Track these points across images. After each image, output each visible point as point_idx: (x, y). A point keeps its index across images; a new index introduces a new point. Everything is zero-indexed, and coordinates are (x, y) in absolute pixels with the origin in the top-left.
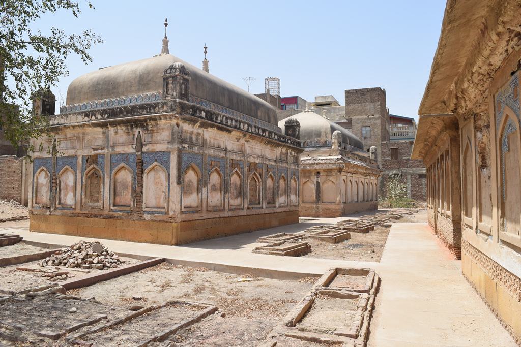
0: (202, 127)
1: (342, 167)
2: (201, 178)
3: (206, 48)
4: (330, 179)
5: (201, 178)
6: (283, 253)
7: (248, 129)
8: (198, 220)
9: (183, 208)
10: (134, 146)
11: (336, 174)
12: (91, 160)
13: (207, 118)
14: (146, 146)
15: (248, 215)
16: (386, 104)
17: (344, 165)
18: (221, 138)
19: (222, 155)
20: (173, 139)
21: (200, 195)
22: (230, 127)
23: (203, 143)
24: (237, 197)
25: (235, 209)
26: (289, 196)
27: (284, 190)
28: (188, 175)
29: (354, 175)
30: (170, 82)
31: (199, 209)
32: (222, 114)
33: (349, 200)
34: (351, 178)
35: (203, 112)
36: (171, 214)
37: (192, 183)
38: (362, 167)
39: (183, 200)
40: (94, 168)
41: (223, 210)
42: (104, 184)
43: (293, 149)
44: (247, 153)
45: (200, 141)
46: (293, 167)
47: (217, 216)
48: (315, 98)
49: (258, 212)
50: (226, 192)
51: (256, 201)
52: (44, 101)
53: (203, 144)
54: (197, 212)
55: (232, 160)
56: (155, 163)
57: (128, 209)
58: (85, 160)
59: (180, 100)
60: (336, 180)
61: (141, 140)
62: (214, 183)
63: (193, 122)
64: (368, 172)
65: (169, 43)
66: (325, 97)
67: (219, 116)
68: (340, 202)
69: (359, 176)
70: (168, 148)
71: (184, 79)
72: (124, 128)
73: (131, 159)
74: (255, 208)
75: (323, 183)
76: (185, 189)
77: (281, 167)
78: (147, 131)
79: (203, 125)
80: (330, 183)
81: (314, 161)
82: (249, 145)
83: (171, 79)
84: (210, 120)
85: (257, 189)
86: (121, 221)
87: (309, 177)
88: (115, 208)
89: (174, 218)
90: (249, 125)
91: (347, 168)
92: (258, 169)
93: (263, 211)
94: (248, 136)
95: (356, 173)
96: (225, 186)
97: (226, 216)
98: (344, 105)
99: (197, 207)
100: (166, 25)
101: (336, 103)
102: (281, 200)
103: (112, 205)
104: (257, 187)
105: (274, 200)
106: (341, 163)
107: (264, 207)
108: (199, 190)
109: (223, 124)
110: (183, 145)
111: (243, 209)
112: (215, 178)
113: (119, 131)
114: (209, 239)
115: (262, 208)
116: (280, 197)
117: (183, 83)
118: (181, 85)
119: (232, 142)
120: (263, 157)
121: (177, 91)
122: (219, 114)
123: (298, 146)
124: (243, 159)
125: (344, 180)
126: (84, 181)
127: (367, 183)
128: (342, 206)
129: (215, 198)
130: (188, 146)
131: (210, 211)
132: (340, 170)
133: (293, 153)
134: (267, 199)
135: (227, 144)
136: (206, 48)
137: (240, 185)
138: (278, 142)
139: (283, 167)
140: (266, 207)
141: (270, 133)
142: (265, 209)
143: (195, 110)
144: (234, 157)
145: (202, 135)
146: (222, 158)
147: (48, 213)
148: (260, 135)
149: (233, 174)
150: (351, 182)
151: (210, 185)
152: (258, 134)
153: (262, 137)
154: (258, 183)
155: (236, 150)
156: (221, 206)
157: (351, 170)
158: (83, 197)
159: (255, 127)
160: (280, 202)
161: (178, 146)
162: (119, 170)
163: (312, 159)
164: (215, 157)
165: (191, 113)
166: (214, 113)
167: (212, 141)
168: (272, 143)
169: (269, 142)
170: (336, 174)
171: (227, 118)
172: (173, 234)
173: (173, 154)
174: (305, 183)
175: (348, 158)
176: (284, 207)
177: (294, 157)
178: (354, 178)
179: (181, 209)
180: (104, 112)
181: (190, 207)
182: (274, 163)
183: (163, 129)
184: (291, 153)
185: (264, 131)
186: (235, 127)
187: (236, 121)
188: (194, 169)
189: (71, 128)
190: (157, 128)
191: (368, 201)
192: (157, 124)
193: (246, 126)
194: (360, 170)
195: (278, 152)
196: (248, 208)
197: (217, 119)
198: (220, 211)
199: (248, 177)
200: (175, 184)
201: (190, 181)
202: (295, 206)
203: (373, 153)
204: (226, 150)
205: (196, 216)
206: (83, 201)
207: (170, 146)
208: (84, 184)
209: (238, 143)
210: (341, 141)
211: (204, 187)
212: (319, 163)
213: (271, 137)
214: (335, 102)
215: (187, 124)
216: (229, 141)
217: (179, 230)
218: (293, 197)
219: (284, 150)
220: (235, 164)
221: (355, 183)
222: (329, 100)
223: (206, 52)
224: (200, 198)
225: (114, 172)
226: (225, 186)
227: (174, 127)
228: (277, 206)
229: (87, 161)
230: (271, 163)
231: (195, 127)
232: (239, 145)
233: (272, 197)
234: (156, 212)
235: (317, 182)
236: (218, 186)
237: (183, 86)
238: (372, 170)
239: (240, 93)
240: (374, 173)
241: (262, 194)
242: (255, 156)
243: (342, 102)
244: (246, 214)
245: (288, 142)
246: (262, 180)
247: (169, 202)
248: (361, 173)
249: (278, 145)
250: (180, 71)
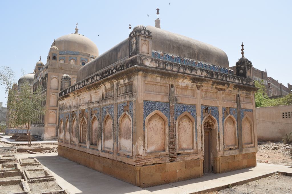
3: (158, 10)
15: (78, 150)
77: (105, 105)
97: (76, 149)
107: (88, 147)
133: (122, 81)
136: (158, 10)
139: (108, 105)
140: (90, 148)
176: (109, 152)
177: (125, 85)
182: (97, 105)
195: (101, 91)
219: (108, 85)
223: (158, 13)
230: (94, 105)
244: (77, 150)
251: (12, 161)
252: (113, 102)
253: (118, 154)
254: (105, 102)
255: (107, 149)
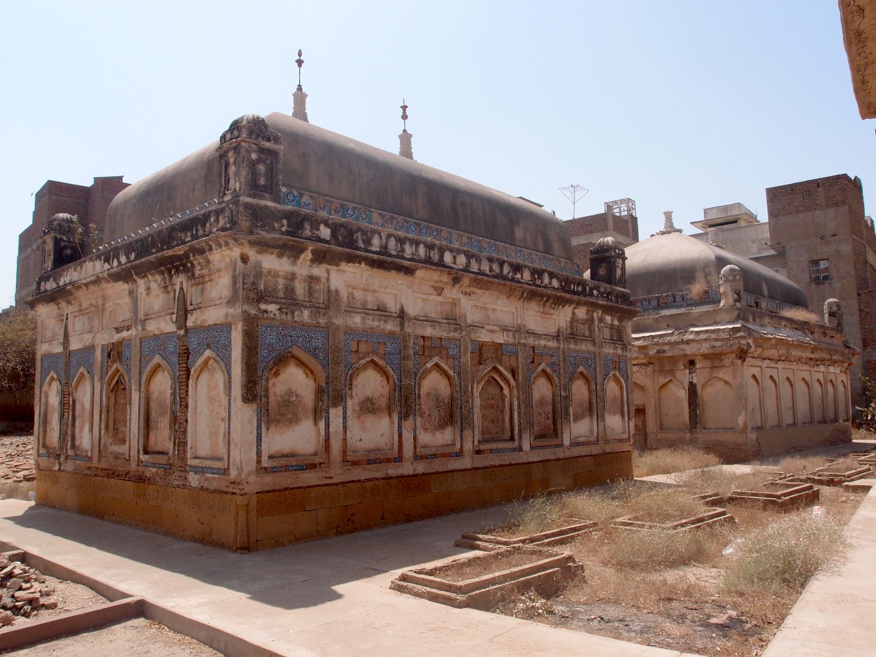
0: (321, 262)
1: (745, 348)
2: (323, 385)
3: (404, 108)
4: (720, 376)
5: (323, 385)
6: (460, 597)
7: (468, 264)
8: (318, 486)
9: (265, 458)
10: (174, 316)
11: (733, 364)
12: (114, 352)
13: (337, 240)
14: (192, 314)
15: (477, 468)
16: (864, 210)
17: (750, 341)
18: (386, 287)
19: (390, 326)
20: (235, 291)
21: (322, 424)
22: (410, 260)
23: (329, 300)
24: (442, 426)
25: (435, 456)
26: (601, 418)
27: (587, 405)
28: (283, 377)
29: (780, 365)
30: (232, 160)
31: (317, 460)
32: (383, 233)
33: (772, 420)
34: (769, 372)
35: (322, 227)
36: (233, 474)
37: (297, 396)
38: (801, 346)
39: (264, 439)
40: (117, 371)
41: (399, 459)
42: (130, 404)
43: (607, 310)
44: (469, 321)
45: (321, 298)
46: (609, 350)
47: (378, 475)
48: (705, 213)
49: (506, 459)
50: (405, 415)
51: (497, 433)
52: (57, 242)
53: (332, 300)
54: (312, 466)
55: (423, 337)
56: (208, 353)
57: (163, 459)
58: (106, 354)
59: (249, 200)
60: (734, 377)
61: (185, 301)
62: (369, 393)
63: (293, 251)
64: (817, 355)
65: (412, 139)
66: (726, 208)
67: (376, 236)
68: (745, 427)
69: (794, 366)
70: (227, 315)
71: (261, 150)
72: (158, 278)
73: (171, 347)
74: (498, 451)
75: (703, 386)
76: (271, 413)
77: (575, 350)
78: (195, 279)
79: (320, 257)
80: (720, 385)
81: (681, 337)
82: (472, 303)
83: (231, 154)
84: (347, 246)
85: (504, 406)
86: (155, 487)
87: (672, 372)
88: (147, 456)
89: (239, 483)
90: (469, 256)
91: (759, 350)
92: (505, 359)
93: (522, 458)
94: (466, 281)
95: (787, 360)
96: (404, 402)
98: (767, 221)
99: (315, 454)
100: (300, 63)
101: (751, 219)
102: (579, 429)
103: (141, 452)
104: (503, 401)
105: (555, 430)
106: (741, 337)
107: (526, 446)
108: (319, 413)
109: (391, 256)
110: (263, 306)
111: (460, 454)
112: (370, 384)
113: (153, 285)
114: (354, 530)
115: (520, 449)
116: (575, 421)
117: (259, 161)
118: (253, 165)
119: (420, 296)
120: (519, 330)
121: (242, 179)
122: (373, 232)
123: (622, 303)
124: (457, 335)
125: (754, 376)
126: (104, 399)
127: (818, 380)
128: (752, 436)
129: (374, 433)
130: (280, 309)
131: (355, 463)
132: (742, 354)
133: (608, 319)
134: (536, 428)
135: (403, 301)
136: (404, 108)
137: (452, 398)
138: (559, 294)
140: (532, 448)
141: (537, 273)
142: (527, 450)
143: (297, 222)
144: (429, 331)
145: (323, 280)
146: (392, 334)
147: (57, 468)
148: (505, 278)
149: (430, 371)
150: (820, 383)
151: (356, 400)
152: (500, 276)
153: (508, 283)
154: (506, 391)
155: (433, 315)
156: (392, 448)
157: (773, 353)
158: (103, 432)
159: (490, 260)
160: (574, 434)
161: (246, 307)
162: (154, 371)
163: (676, 332)
164: (367, 333)
165: (284, 229)
166: (359, 229)
167: (359, 295)
168: (542, 296)
169: (533, 295)
170: (733, 364)
171: (401, 241)
172: (237, 524)
173: (236, 329)
174: (664, 386)
175: (762, 326)
176: (588, 443)
177: (612, 327)
178: (781, 371)
179: (259, 462)
180: (129, 248)
181: (292, 455)
182: (552, 344)
183: (219, 271)
184: (601, 320)
185: (517, 268)
186: (428, 261)
187: (430, 247)
188: (301, 363)
189: (84, 288)
190: (209, 270)
191: (825, 422)
192: (208, 262)
193: (462, 260)
194: (795, 353)
195: (562, 317)
196: (478, 452)
197: (368, 242)
198: (388, 461)
199: (473, 377)
200: (239, 400)
201: (290, 393)
202: (621, 441)
203: (832, 314)
204: (402, 315)
205: (311, 478)
206: (102, 442)
207: (231, 311)
208: (104, 405)
209: (440, 299)
210: (742, 287)
211: (335, 405)
212: (692, 341)
213: (538, 282)
214: (746, 217)
215: (274, 256)
216: (413, 296)
217: (253, 514)
218: (614, 423)
220: (429, 347)
221: (787, 384)
222: (735, 212)
223: (405, 117)
224: (323, 432)
225: (144, 377)
226: (404, 402)
227: (236, 265)
228: (567, 442)
229: (109, 355)
230: (543, 343)
231: (299, 262)
232: (442, 303)
233: (550, 421)
234: (209, 468)
235: (691, 383)
236: (384, 402)
237: (261, 168)
238: (830, 352)
239: (462, 185)
240: (834, 358)
241: (519, 417)
242: (495, 328)
243: (763, 216)
244: (469, 466)
245: (591, 294)
246: (517, 384)
247: (229, 445)
248: (799, 360)
249: (559, 302)
250: (251, 133)
251: (573, 538)
252: (593, 349)
253: (607, 442)
254: (576, 344)
255: (583, 439)
